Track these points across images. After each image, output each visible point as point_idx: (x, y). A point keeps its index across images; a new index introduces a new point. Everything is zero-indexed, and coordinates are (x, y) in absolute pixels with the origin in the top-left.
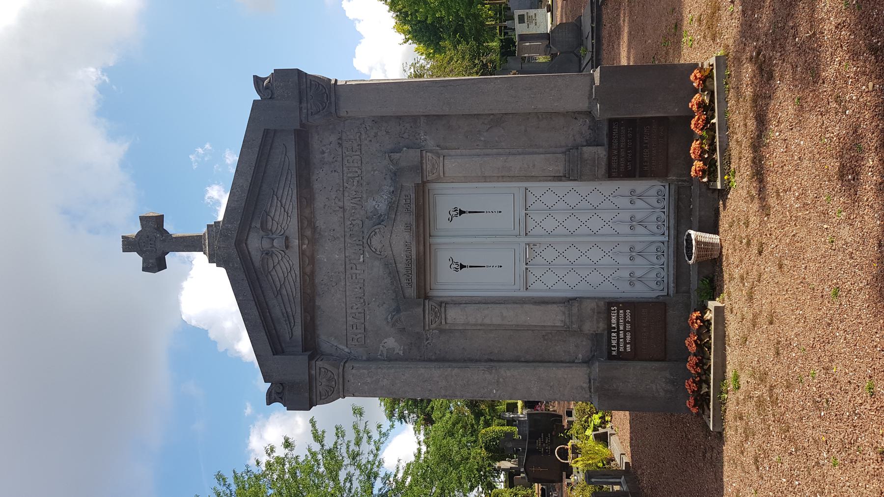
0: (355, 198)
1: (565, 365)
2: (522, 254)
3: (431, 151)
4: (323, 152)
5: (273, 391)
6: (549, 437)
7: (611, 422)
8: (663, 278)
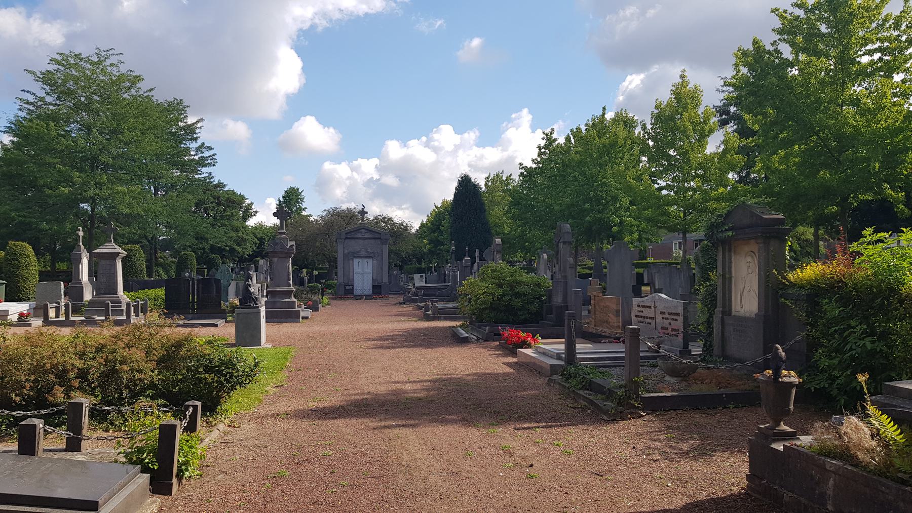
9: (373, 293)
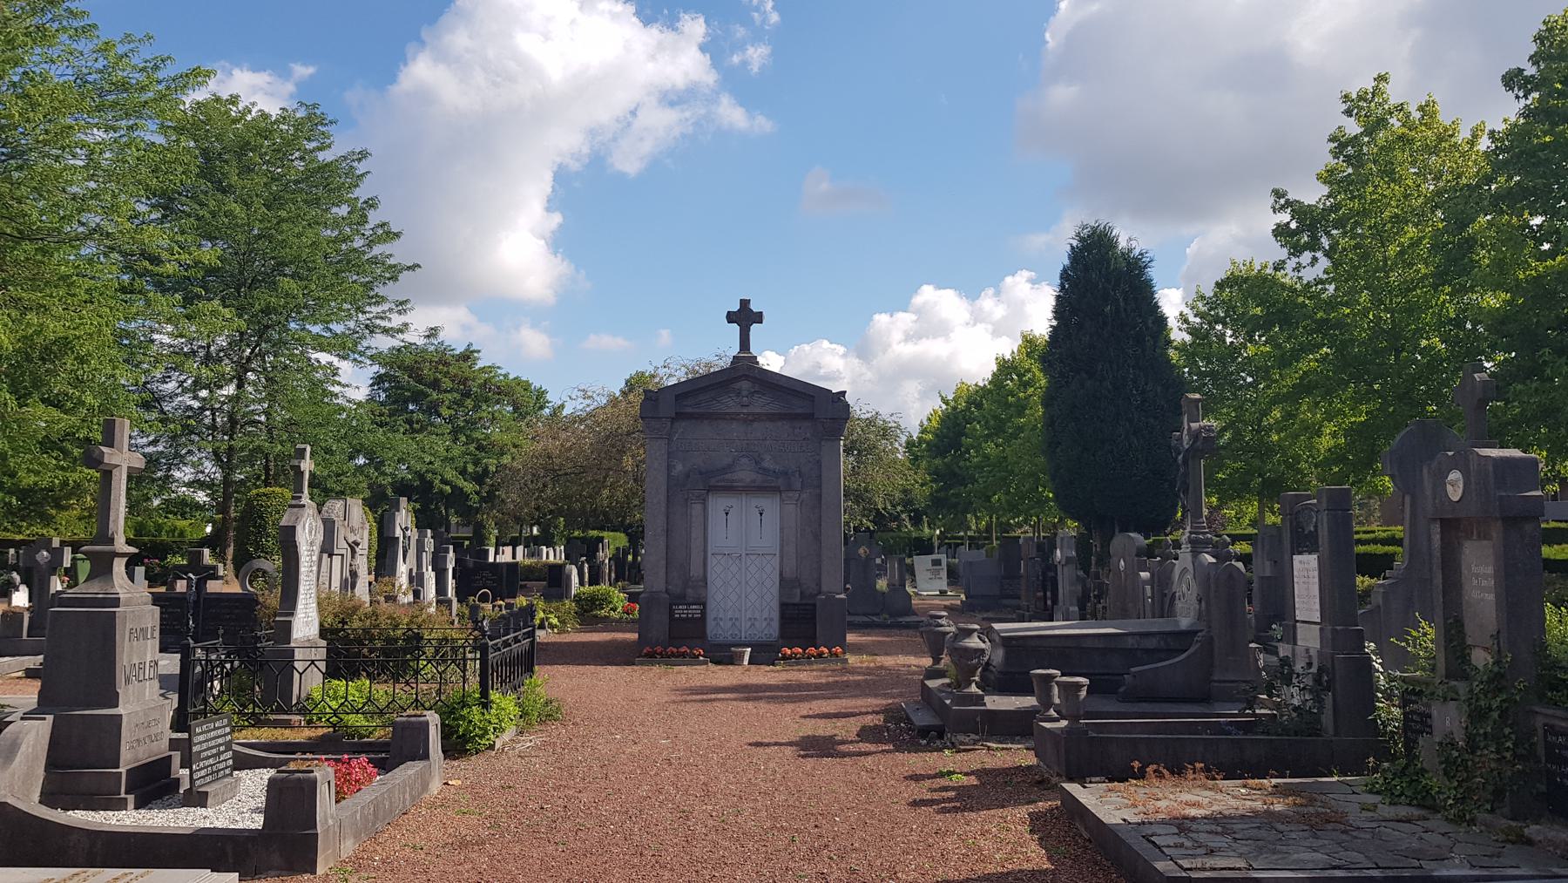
4: (800, 428)
9: (783, 635)
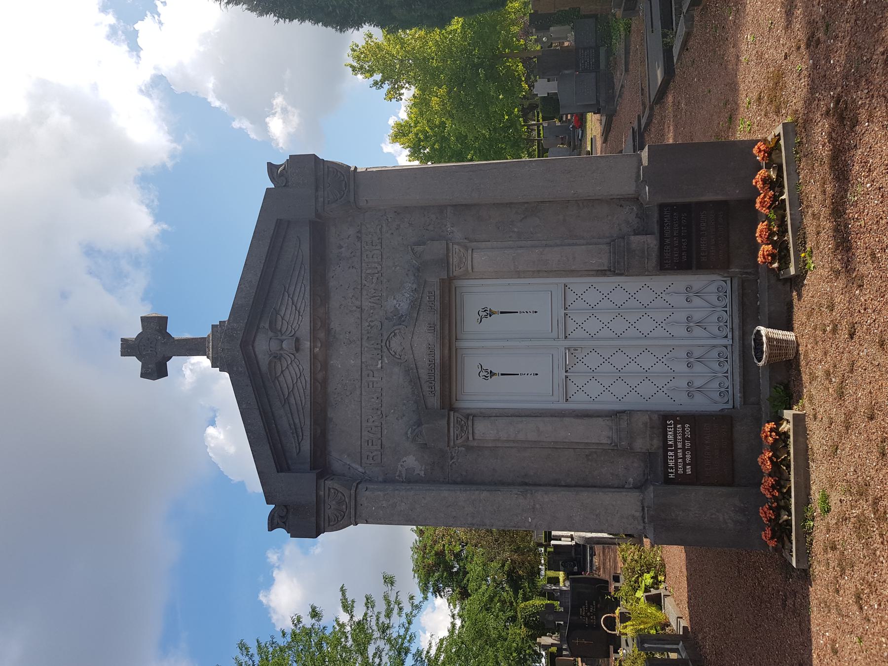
0: (375, 297)
1: (613, 490)
2: (561, 360)
3: (458, 244)
4: (341, 247)
5: (276, 515)
6: (594, 604)
7: (664, 582)
8: (727, 388)
